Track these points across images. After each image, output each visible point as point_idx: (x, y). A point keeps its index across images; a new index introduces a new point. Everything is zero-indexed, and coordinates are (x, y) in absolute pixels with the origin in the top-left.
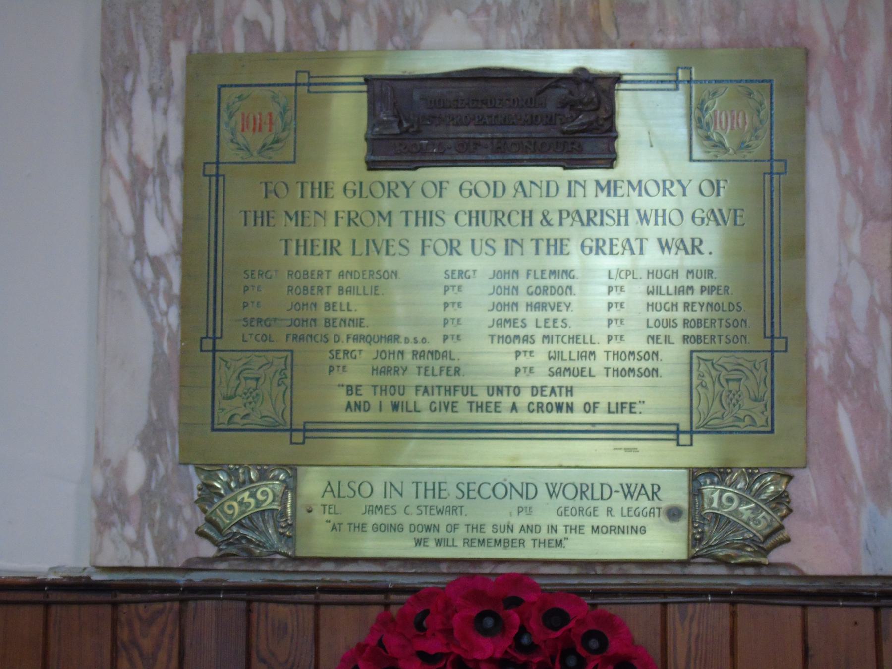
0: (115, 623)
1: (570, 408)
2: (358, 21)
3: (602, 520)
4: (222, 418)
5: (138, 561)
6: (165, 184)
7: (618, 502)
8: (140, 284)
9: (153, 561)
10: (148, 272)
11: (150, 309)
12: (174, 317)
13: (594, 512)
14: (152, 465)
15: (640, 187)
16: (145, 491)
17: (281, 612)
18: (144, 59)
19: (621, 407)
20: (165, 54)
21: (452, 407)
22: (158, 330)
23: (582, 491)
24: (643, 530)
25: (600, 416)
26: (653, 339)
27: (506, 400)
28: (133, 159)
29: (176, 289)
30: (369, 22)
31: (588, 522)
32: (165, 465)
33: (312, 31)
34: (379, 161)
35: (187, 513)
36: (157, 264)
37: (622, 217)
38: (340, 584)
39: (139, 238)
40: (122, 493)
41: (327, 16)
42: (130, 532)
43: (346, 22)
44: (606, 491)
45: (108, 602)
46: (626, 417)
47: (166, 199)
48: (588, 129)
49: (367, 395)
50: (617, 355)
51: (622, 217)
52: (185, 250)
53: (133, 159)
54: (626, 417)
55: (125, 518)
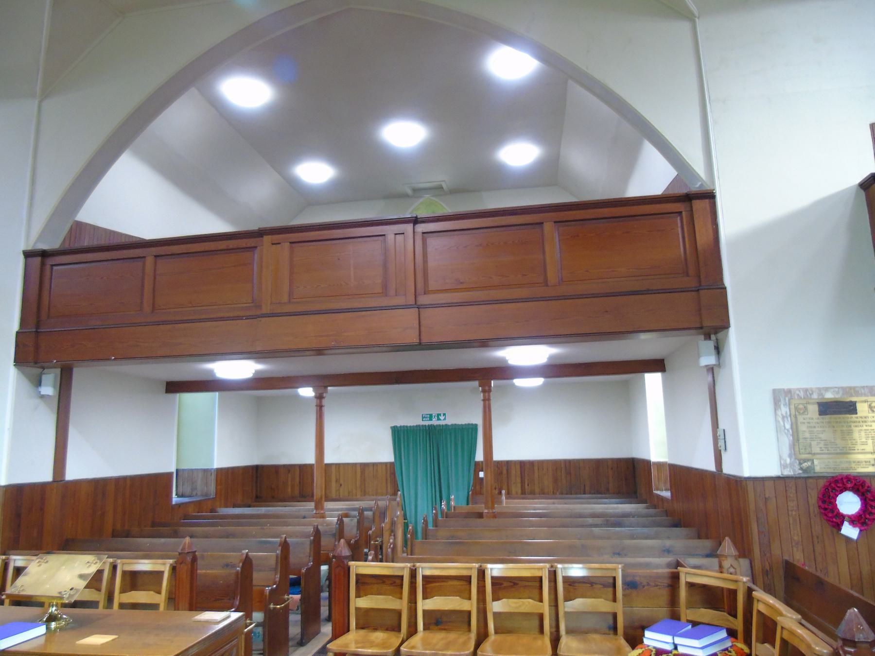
0: (785, 482)
1: (855, 450)
2: (814, 393)
3: (862, 466)
4: (801, 453)
5: (790, 474)
6: (787, 418)
7: (864, 463)
8: (785, 433)
9: (792, 474)
10: (786, 431)
11: (788, 437)
12: (791, 438)
13: (860, 465)
14: (791, 459)
15: (861, 417)
16: (790, 464)
17: (811, 480)
18: (782, 399)
19: (863, 450)
20: (785, 399)
21: (837, 450)
22: (789, 440)
23: (858, 462)
24: (868, 467)
25: (860, 451)
26: (866, 439)
27: (845, 449)
28: (782, 415)
29: (791, 433)
30: (788, 420)
31: (860, 466)
32: (793, 460)
33: (807, 395)
34: (646, 538)
35: (797, 466)
36: (788, 430)
37: (859, 422)
38: (617, 511)
39: (784, 426)
40: (786, 464)
41: (810, 393)
42: (788, 469)
43: (812, 394)
44: (862, 462)
45: (816, 473)
46: (863, 451)
47: (788, 420)
48: (853, 409)
49: (823, 449)
50: (861, 442)
51: (859, 422)
52: (792, 428)
53: (782, 415)
54: (863, 451)
55: (787, 468)
